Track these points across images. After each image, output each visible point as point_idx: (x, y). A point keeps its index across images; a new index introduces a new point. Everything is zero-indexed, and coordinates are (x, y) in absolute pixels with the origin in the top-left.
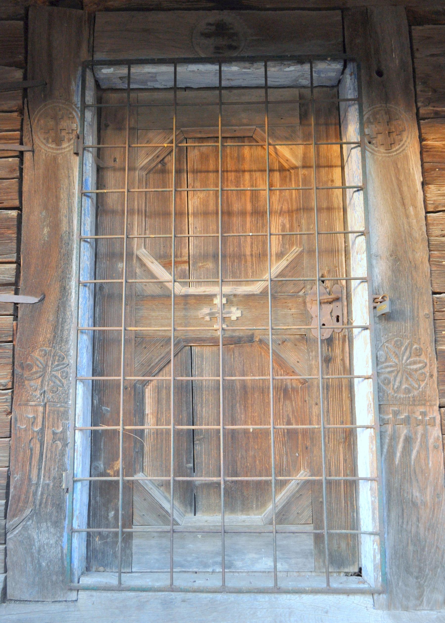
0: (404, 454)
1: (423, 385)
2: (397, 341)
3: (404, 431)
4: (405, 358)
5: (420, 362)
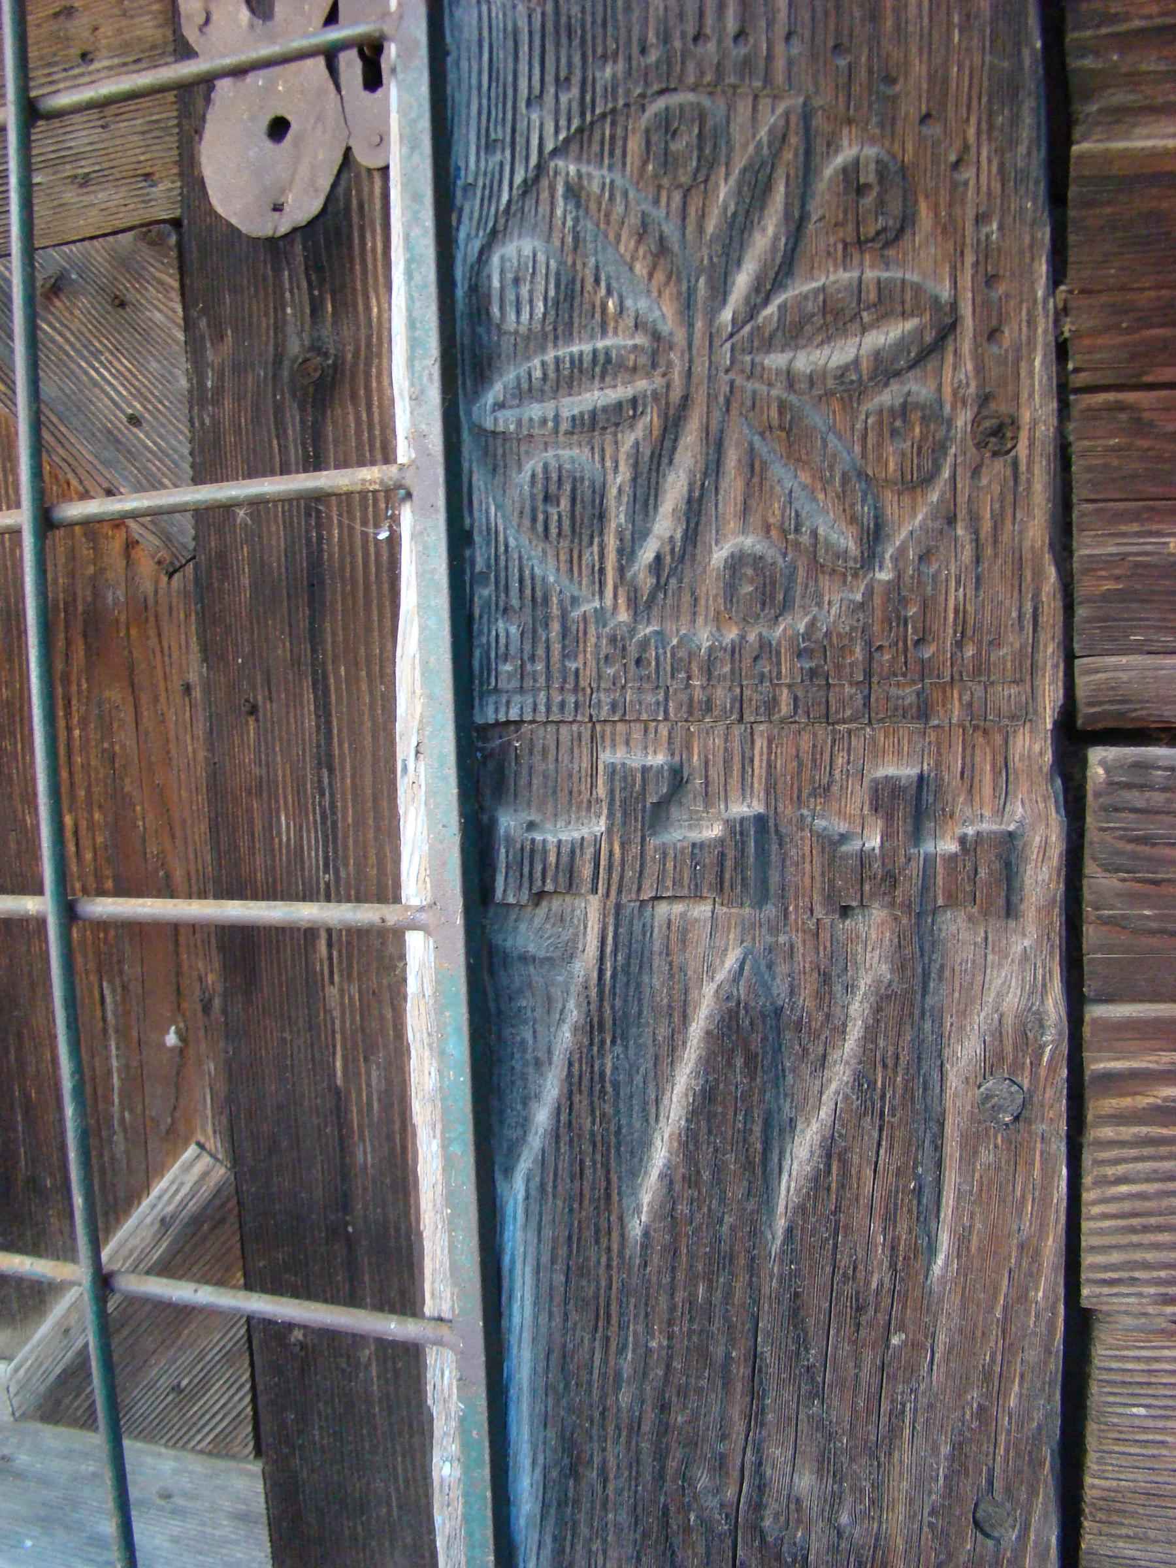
0: (705, 1155)
1: (909, 523)
2: (667, 125)
3: (715, 956)
4: (742, 281)
5: (887, 302)
